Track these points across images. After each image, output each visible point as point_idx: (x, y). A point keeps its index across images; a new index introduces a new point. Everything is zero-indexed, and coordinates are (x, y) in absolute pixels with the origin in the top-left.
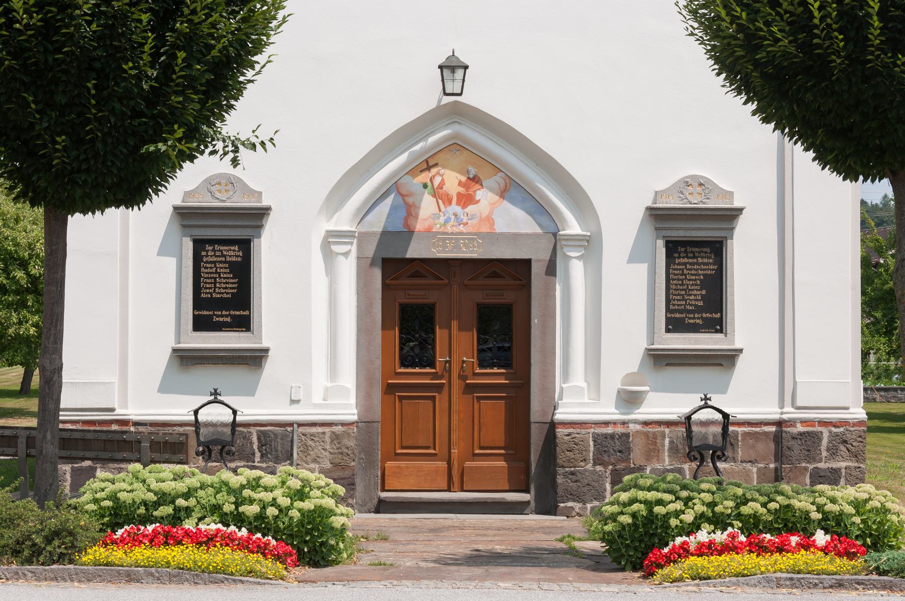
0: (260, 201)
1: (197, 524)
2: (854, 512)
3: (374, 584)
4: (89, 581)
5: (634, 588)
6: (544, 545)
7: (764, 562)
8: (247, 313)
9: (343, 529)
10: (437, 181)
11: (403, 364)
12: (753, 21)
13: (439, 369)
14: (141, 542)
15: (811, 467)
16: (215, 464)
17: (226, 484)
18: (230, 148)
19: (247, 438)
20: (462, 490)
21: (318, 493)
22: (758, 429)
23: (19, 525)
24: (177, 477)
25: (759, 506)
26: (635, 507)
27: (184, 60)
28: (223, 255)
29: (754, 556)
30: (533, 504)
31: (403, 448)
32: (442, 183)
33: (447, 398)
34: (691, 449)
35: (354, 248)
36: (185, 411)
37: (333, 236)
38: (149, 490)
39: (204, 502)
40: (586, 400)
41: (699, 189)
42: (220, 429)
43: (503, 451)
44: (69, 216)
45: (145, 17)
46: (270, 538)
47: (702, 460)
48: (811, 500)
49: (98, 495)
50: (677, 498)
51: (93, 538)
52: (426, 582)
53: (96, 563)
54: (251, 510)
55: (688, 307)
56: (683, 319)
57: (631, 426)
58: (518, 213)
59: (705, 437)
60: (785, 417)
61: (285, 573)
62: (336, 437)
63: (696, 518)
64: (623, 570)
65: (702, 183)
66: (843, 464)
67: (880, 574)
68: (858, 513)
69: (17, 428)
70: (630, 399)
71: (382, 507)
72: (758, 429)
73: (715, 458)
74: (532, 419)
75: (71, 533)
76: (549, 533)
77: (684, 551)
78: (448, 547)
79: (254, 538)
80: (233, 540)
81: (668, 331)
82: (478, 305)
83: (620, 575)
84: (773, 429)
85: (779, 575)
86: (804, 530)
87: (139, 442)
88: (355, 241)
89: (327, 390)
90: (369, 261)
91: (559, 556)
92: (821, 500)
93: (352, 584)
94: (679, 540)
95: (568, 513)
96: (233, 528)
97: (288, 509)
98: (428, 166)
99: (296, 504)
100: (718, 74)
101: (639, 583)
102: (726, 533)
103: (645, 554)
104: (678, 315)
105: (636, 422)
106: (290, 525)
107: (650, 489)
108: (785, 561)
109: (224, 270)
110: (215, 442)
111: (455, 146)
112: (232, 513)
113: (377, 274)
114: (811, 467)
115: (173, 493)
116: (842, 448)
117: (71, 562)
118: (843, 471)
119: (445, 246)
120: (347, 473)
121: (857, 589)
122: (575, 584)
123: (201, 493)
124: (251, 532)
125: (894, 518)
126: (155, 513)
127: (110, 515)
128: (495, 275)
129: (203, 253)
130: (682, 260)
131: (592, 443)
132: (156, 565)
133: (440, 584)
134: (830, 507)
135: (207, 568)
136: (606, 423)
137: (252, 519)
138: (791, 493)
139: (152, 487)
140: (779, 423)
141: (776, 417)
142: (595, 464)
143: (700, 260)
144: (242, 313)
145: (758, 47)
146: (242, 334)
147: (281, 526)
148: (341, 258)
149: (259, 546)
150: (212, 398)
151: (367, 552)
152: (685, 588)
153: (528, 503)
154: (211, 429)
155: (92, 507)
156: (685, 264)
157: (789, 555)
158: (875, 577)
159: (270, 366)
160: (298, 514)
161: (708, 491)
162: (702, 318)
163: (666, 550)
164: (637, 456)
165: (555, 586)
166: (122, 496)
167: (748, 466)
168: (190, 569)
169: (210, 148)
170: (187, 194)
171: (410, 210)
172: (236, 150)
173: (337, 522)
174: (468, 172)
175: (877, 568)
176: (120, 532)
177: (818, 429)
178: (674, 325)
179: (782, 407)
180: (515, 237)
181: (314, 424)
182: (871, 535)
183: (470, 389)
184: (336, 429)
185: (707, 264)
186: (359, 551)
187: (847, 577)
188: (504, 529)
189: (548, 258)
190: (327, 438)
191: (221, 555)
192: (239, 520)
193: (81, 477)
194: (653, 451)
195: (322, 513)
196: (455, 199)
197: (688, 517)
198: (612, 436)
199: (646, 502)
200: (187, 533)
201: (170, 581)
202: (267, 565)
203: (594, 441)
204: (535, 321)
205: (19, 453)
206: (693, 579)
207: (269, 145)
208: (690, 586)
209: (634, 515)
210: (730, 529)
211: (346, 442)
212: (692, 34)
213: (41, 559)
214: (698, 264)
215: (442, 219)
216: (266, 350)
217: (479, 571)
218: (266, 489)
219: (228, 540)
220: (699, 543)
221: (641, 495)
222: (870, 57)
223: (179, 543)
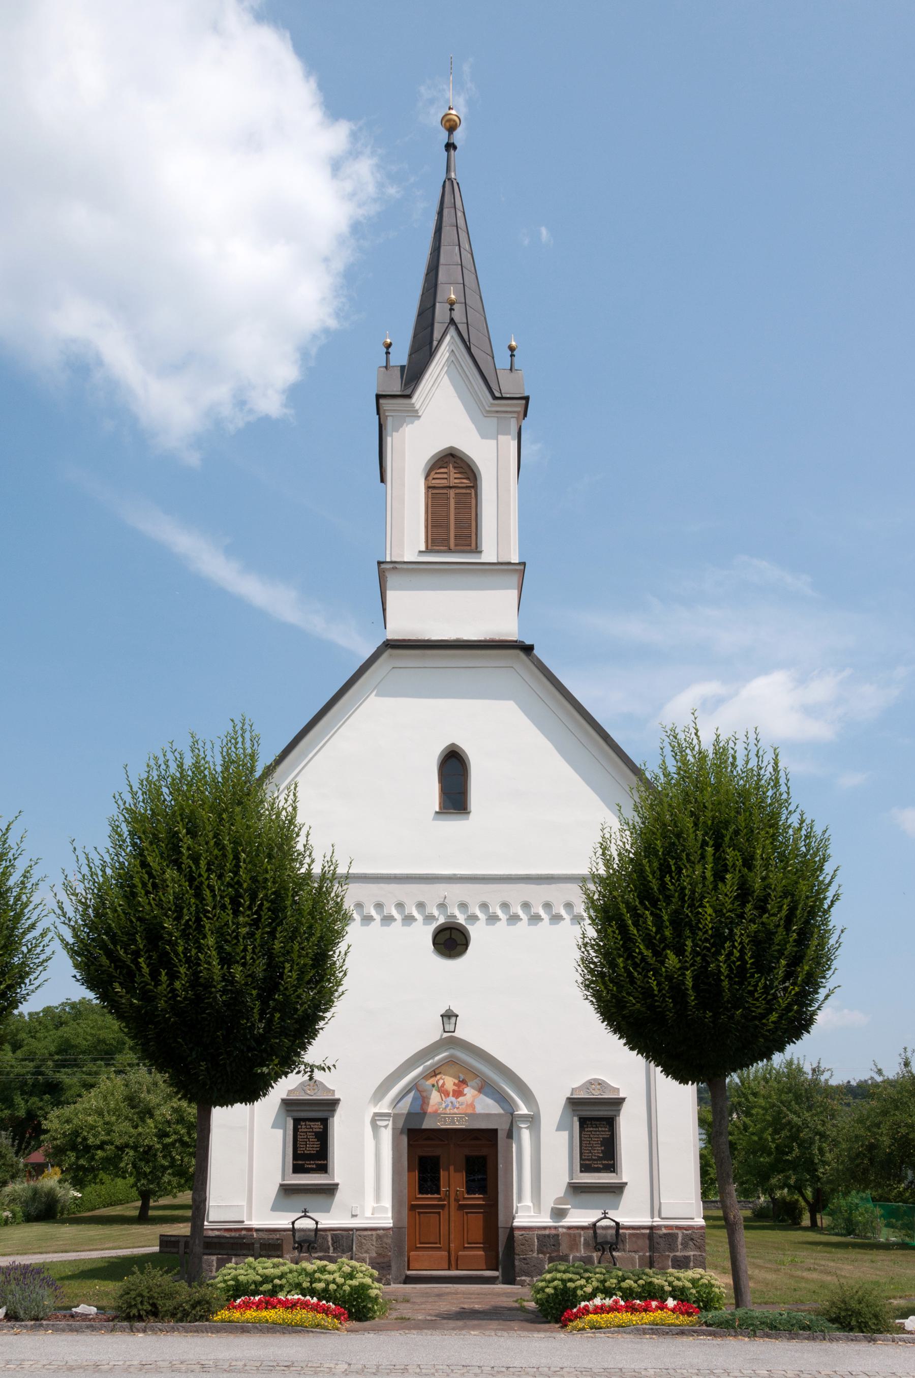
0: (334, 1095)
1: (287, 1295)
2: (691, 1286)
3: (393, 1333)
4: (218, 1332)
5: (554, 1335)
6: (505, 1305)
7: (635, 1318)
8: (325, 1162)
9: (377, 1297)
10: (441, 1082)
11: (421, 1192)
12: (621, 992)
13: (442, 1195)
14: (251, 1307)
15: (672, 1255)
16: (305, 1255)
17: (304, 1270)
18: (309, 1069)
19: (325, 1238)
20: (457, 1269)
21: (361, 1275)
22: (638, 1232)
23: (175, 1297)
24: (275, 1266)
25: (632, 1282)
26: (556, 1283)
27: (278, 1019)
28: (311, 1128)
29: (629, 1314)
30: (501, 1278)
31: (421, 1243)
32: (444, 1084)
33: (447, 1212)
34: (597, 1244)
35: (390, 1123)
36: (286, 1222)
37: (377, 1116)
38: (258, 1274)
39: (291, 1281)
40: (533, 1214)
41: (598, 1087)
42: (308, 1233)
43: (482, 1245)
44: (213, 1108)
45: (254, 992)
46: (331, 1304)
47: (604, 1251)
48: (665, 1279)
49: (226, 1278)
50: (582, 1277)
51: (221, 1306)
52: (426, 1331)
53: (223, 1321)
54: (320, 1286)
55: (594, 1157)
56: (591, 1164)
57: (560, 1230)
58: (490, 1102)
59: (605, 1236)
60: (655, 1224)
61: (339, 1326)
62: (379, 1237)
63: (593, 1290)
64: (549, 1322)
65: (601, 1083)
66: (692, 1253)
67: (707, 1326)
68: (694, 1287)
69: (179, 1236)
70: (559, 1214)
71: (408, 1280)
72: (638, 1232)
73: (612, 1249)
74: (499, 1226)
75: (208, 1302)
76: (510, 1297)
77: (586, 1311)
78: (445, 1306)
79: (321, 1303)
80: (308, 1306)
81: (581, 1171)
82: (466, 1156)
83: (547, 1326)
84: (648, 1231)
85: (644, 1326)
86: (661, 1297)
87: (253, 1244)
88: (391, 1119)
89: (374, 1209)
90: (400, 1130)
91: (514, 1312)
92: (671, 1279)
93: (380, 1333)
94: (583, 1304)
95: (522, 1284)
96: (308, 1298)
97: (343, 1285)
98: (435, 1074)
99: (347, 1282)
100: (603, 1022)
101: (558, 1332)
102: (612, 1299)
103: (562, 1312)
104: (587, 1162)
105: (563, 1227)
106: (344, 1295)
107: (564, 1272)
108: (648, 1317)
109: (311, 1137)
110: (305, 1241)
111: (451, 1062)
112: (308, 1288)
113: (405, 1139)
114: (672, 1255)
115: (272, 1276)
116: (691, 1243)
117: (207, 1320)
118: (692, 1257)
119: (445, 1121)
120: (386, 1260)
121: (693, 1336)
122: (518, 1332)
123: (290, 1276)
124: (320, 1300)
125: (717, 1290)
126: (261, 1289)
127: (233, 1290)
128: (476, 1139)
129: (299, 1127)
130: (589, 1129)
131: (536, 1240)
132: (260, 1321)
133: (434, 1332)
134: (676, 1283)
135: (291, 1323)
136: (545, 1228)
137: (320, 1292)
138: (652, 1275)
139: (259, 1272)
140: (651, 1228)
141: (650, 1224)
142: (538, 1253)
143: (600, 1129)
144: (322, 1162)
145: (625, 1007)
146: (322, 1175)
147: (338, 1295)
148: (383, 1129)
149: (324, 1309)
150: (303, 1214)
151: (396, 1310)
152: (586, 1335)
153: (497, 1277)
154: (303, 1233)
155: (222, 1285)
156: (591, 1131)
157: (651, 1313)
158: (704, 1328)
159: (339, 1195)
160: (349, 1288)
161: (601, 1273)
162: (602, 1164)
163: (575, 1310)
164: (564, 1249)
165: (505, 1334)
166: (241, 1278)
167: (633, 1254)
168: (280, 1324)
169: (297, 1070)
170: (290, 1092)
171: (423, 1099)
172: (312, 1071)
173: (373, 1292)
174: (459, 1077)
175: (706, 1322)
176: (238, 1301)
177: (676, 1231)
178: (586, 1168)
179: (653, 1218)
180: (488, 1116)
181: (366, 1229)
182: (703, 1301)
183: (461, 1207)
184: (379, 1232)
185: (604, 1131)
186: (390, 1309)
187: (687, 1328)
188: (482, 1294)
189: (508, 1128)
190: (374, 1238)
191: (301, 1315)
192: (313, 1292)
193: (221, 1264)
194: (574, 1245)
195: (363, 1287)
196: (451, 1094)
197: (589, 1289)
198: (549, 1236)
199: (562, 1280)
200: (280, 1301)
201: (268, 1332)
202: (329, 1321)
203: (538, 1239)
204: (500, 1166)
205: (180, 1252)
206: (591, 1328)
207: (332, 1068)
208: (589, 1334)
209: (555, 1288)
210: (614, 1297)
211: (385, 1240)
212: (587, 999)
213: (189, 1319)
214: (599, 1131)
215: (444, 1105)
216: (337, 1185)
217: (460, 1323)
218: (330, 1273)
219: (305, 1305)
220: (595, 1306)
221: (559, 1275)
222: (689, 1013)
223: (274, 1307)
